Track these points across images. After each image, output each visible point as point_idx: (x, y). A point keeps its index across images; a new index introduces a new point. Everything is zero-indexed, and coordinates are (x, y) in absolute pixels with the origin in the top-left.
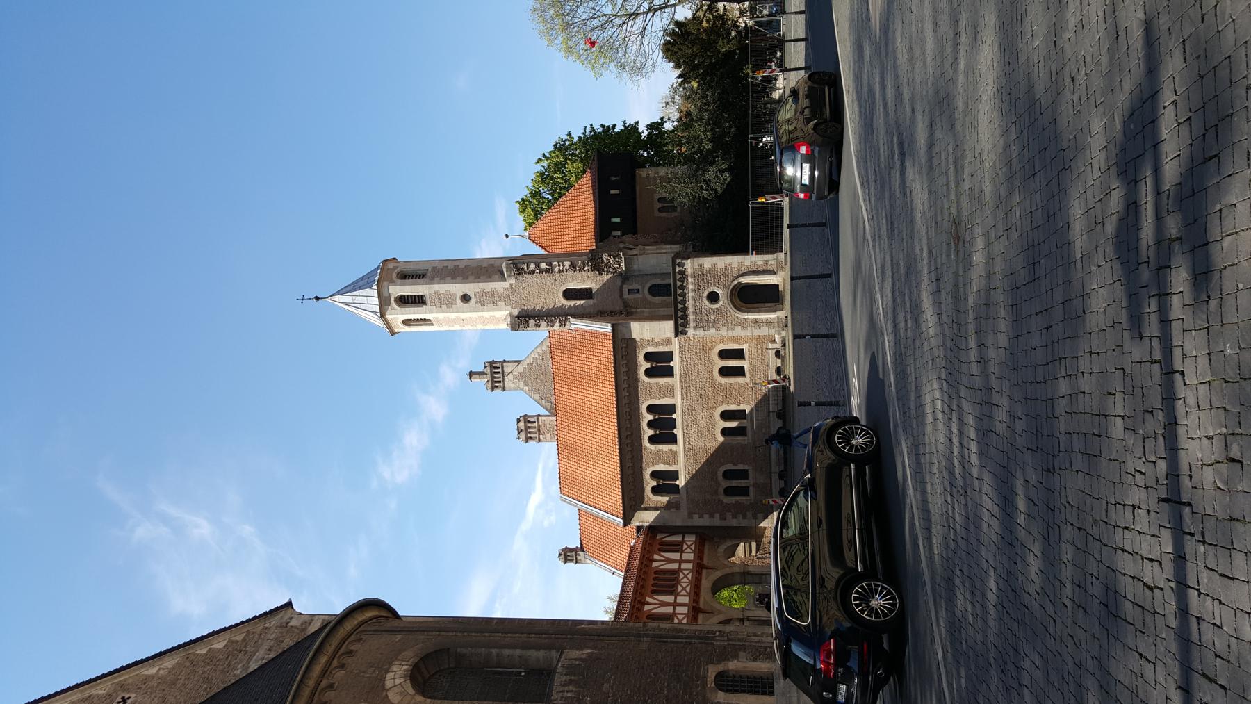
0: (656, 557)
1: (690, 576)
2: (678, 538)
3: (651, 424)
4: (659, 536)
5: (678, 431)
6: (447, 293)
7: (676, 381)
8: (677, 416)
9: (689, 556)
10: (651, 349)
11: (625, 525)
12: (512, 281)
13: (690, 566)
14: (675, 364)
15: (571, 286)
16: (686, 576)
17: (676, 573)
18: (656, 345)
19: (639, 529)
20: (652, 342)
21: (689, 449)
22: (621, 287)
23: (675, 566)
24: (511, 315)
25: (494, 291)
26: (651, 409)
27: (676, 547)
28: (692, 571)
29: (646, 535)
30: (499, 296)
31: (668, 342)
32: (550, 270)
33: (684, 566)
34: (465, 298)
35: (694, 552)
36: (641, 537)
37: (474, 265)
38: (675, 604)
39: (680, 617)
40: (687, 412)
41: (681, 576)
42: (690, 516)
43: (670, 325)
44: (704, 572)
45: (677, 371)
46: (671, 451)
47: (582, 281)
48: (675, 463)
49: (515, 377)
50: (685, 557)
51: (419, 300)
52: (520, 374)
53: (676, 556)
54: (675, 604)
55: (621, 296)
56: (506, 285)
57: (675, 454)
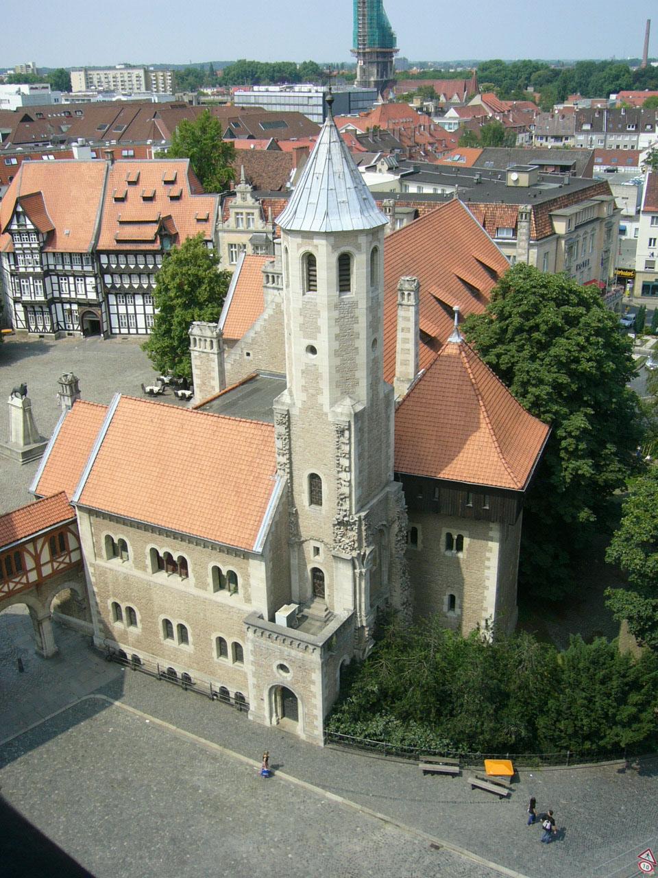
6: (318, 330)
25: (319, 391)
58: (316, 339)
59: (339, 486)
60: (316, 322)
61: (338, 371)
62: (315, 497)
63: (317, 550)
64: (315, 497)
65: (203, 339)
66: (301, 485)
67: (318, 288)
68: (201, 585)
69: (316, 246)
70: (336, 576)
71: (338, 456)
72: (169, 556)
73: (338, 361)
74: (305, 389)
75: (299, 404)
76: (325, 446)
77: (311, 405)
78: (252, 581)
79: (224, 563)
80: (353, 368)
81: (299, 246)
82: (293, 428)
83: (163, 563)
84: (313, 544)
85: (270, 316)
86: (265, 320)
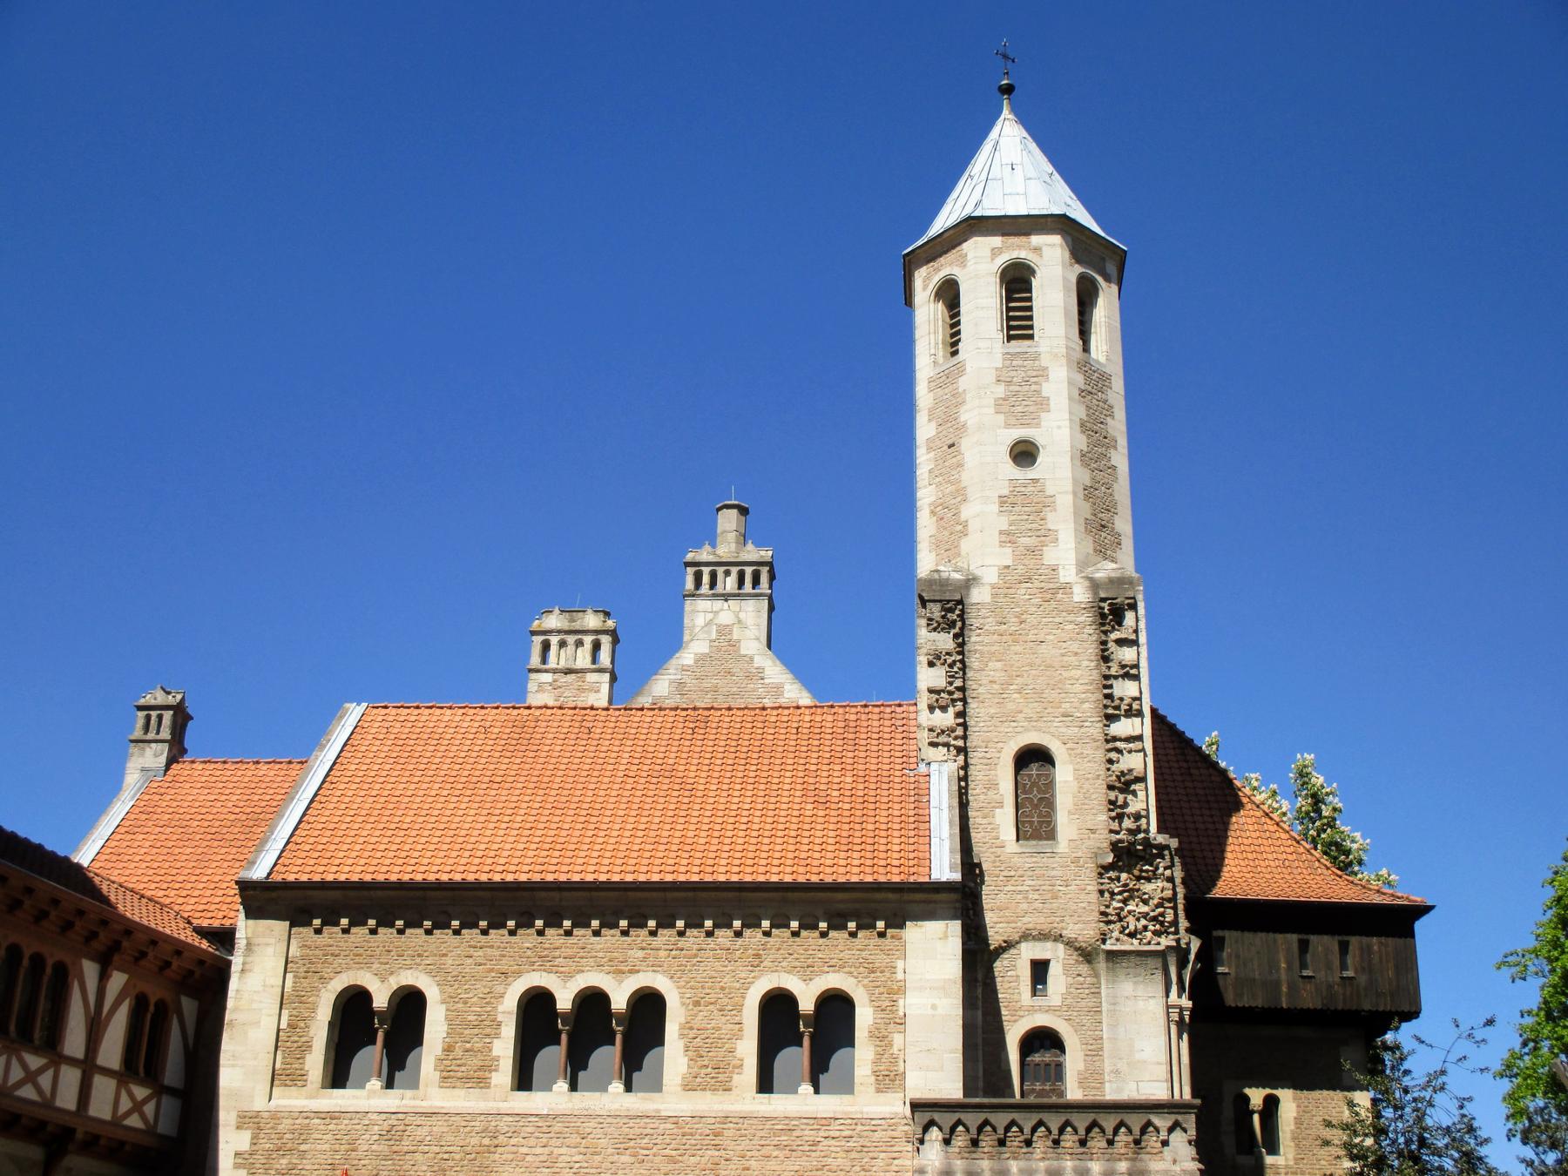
0: (118, 980)
1: (27, 1092)
2: (173, 1072)
3: (593, 1001)
4: (189, 1006)
5: (554, 1098)
6: (1043, 404)
7: (743, 1096)
8: (614, 1098)
9: (105, 1100)
10: (864, 1017)
11: (245, 887)
12: (1081, 594)
13: (67, 1099)
14: (800, 1102)
15: (1064, 774)
16: (31, 1077)
17: (51, 1044)
18: (881, 1038)
19: (224, 938)
20: (893, 1020)
21: (491, 1130)
22: (1058, 938)
23: (74, 1042)
24: (970, 582)
25: (1047, 536)
26: (649, 1006)
27: (141, 1060)
28: (48, 1104)
29: (201, 960)
30: (1033, 551)
31: (889, 1079)
32: (960, 780)
33: (70, 1078)
34: (1024, 454)
35: (116, 1122)
36: (188, 936)
37: (333, 1054)
38: (89, 1066)
39: (45, 1080)
40: (632, 1137)
41: (34, 1062)
42: (248, 1120)
43: (950, 1086)
44: (35, 1153)
45: (777, 1104)
46: (489, 1066)
47: (1078, 810)
48: (448, 1078)
49: (724, 630)
50: (104, 1088)
51: (1018, 324)
52: (734, 645)
53: (111, 1052)
54: (89, 1066)
55: (1026, 936)
56: (1068, 574)
57: (479, 1079)
58: (1038, 425)
59: (1113, 755)
60: (1038, 392)
61: (1087, 498)
62: (1035, 820)
63: (1040, 970)
64: (1035, 820)
65: (571, 639)
66: (992, 785)
67: (1036, 332)
68: (711, 1073)
69: (1037, 250)
70: (1113, 1027)
71: (1106, 677)
72: (593, 1001)
73: (1086, 477)
74: (1008, 538)
75: (990, 576)
76: (1065, 667)
77: (1028, 571)
78: (913, 1004)
79: (807, 972)
80: (1110, 508)
81: (995, 252)
82: (973, 639)
83: (569, 1036)
84: (1029, 952)
85: (701, 659)
86: (684, 669)
